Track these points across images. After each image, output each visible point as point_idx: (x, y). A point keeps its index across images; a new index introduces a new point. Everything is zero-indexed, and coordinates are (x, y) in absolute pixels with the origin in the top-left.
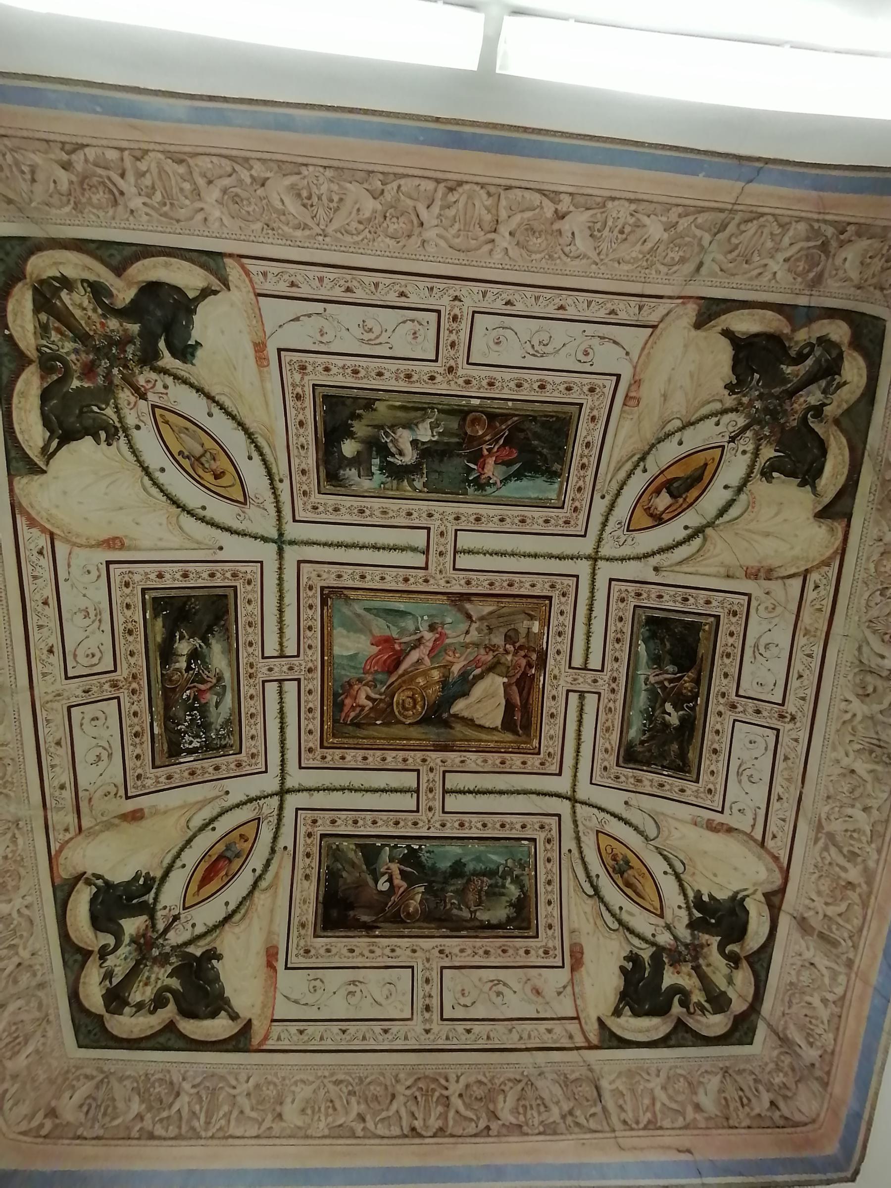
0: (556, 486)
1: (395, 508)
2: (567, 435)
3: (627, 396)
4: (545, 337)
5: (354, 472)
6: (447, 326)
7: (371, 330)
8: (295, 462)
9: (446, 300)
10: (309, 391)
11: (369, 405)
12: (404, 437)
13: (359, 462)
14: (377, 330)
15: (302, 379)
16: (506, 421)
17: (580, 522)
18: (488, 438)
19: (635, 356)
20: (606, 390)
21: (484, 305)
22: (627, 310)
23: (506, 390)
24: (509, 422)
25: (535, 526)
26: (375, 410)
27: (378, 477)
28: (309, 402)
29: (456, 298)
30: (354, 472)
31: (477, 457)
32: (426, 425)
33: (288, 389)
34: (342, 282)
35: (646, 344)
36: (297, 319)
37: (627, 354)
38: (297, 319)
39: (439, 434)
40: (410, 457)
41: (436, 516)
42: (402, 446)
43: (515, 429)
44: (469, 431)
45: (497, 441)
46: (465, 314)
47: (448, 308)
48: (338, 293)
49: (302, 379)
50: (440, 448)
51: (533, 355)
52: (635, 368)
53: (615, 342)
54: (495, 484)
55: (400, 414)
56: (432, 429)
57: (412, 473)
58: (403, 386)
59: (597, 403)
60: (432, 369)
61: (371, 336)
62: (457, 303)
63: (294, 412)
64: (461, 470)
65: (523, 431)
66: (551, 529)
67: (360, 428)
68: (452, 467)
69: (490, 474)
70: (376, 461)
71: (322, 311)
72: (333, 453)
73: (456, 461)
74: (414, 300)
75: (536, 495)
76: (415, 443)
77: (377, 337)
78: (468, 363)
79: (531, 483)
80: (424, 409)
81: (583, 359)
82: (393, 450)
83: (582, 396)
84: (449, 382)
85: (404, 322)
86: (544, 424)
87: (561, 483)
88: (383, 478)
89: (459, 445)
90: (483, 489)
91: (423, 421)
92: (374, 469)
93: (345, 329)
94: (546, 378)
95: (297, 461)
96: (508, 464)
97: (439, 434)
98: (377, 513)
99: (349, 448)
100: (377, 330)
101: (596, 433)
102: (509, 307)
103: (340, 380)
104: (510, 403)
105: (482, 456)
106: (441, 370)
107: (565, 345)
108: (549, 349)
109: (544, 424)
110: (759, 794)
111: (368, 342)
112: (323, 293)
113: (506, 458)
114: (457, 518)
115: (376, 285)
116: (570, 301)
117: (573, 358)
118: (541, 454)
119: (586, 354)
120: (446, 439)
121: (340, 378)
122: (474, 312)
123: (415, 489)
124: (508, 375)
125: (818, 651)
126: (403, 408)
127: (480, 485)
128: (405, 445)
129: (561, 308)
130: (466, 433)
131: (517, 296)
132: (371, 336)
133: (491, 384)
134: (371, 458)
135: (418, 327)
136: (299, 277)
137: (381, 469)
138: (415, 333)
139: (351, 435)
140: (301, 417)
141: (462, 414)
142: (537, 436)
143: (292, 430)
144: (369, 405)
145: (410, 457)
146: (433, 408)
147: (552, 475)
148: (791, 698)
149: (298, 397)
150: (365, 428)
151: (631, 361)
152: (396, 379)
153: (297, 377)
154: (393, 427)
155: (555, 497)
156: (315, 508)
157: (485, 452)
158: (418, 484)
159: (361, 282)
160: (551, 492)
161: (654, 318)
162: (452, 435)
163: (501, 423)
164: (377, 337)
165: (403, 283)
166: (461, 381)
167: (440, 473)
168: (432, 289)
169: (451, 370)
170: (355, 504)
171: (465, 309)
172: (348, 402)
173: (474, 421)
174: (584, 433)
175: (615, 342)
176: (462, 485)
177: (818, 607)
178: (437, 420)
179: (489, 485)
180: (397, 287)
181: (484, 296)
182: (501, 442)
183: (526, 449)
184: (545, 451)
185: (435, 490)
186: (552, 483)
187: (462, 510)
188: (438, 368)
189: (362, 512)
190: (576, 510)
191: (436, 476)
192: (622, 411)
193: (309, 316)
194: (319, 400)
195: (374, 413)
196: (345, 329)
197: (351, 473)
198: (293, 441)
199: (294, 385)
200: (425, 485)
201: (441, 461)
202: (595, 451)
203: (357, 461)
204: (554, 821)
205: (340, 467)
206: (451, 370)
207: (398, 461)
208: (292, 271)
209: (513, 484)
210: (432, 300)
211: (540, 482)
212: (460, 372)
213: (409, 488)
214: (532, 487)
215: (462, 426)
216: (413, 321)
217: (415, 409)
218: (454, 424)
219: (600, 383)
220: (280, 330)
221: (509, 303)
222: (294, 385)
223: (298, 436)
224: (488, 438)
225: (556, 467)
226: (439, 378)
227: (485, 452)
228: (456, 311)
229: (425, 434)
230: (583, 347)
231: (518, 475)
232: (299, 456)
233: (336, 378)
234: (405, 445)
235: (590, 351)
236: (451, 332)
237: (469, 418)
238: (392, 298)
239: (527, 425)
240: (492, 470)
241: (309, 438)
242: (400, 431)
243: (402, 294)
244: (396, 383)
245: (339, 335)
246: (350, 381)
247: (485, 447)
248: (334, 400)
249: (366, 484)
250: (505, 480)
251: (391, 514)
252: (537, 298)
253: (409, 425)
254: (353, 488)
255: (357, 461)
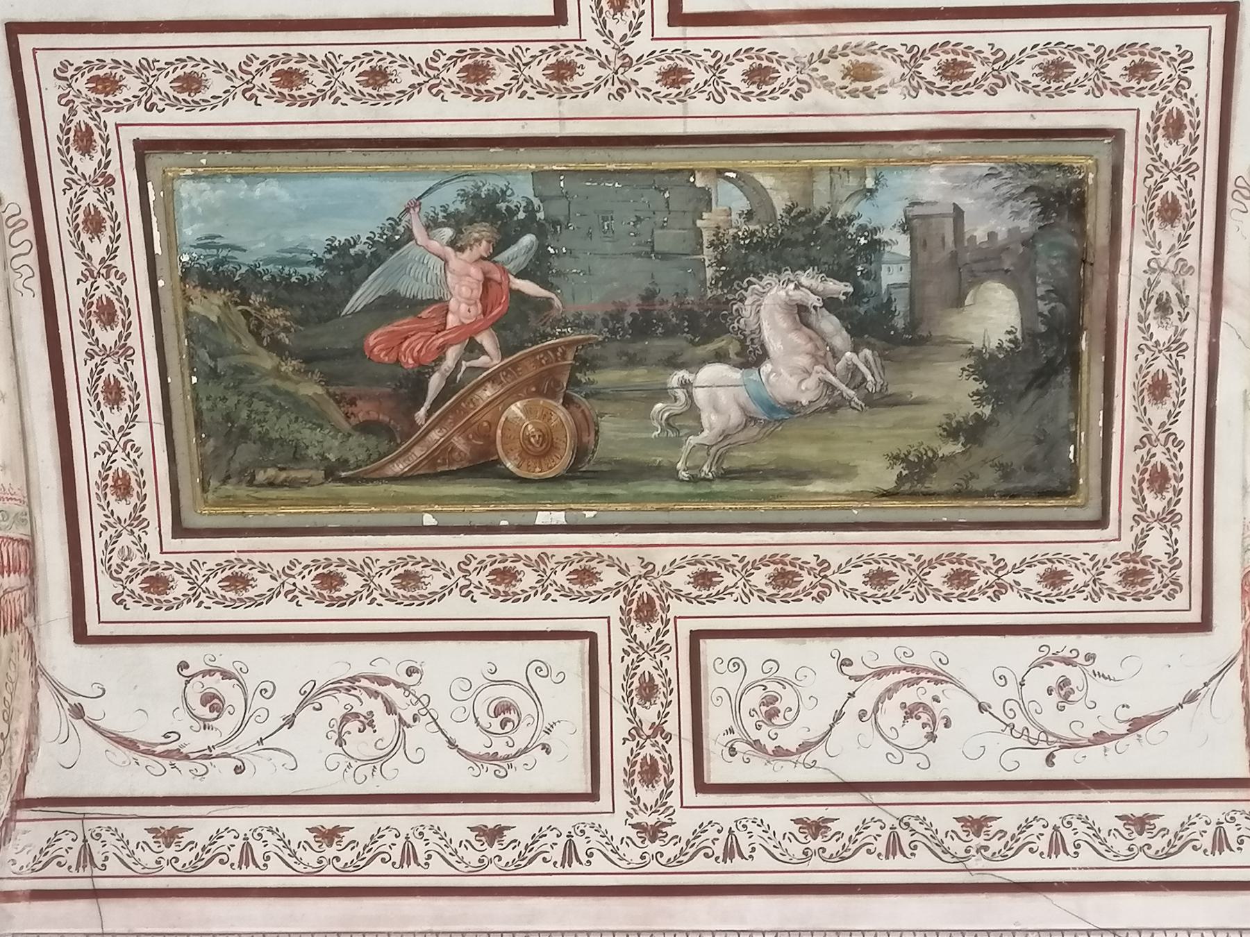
0: (190, 233)
1: (818, 97)
2: (199, 423)
3: (32, 572)
4: (360, 743)
5: (978, 230)
6: (672, 748)
7: (910, 712)
8: (1198, 251)
9: (685, 823)
10: (1123, 505)
11: (916, 476)
12: (789, 373)
13: (958, 267)
14: (891, 714)
15: (1140, 542)
16: (431, 459)
17: (52, 90)
18: (488, 393)
19: (52, 715)
20: (108, 587)
21: (564, 820)
22: (127, 844)
23: (452, 560)
24: (418, 452)
25: (233, 58)
26: (895, 458)
27: (884, 215)
28: (1126, 465)
29: (653, 833)
30: (978, 230)
31: (516, 321)
32: (712, 422)
33: (1189, 505)
34: (996, 845)
35: (29, 747)
36: (1137, 725)
37: (78, 712)
38: (1137, 725)
39: (662, 393)
40: (768, 304)
41: (648, 76)
42: (798, 339)
43: (390, 432)
44: (561, 413)
45: (451, 385)
46: (620, 788)
47: (674, 800)
48: (1008, 813)
49: (1140, 542)
50: (658, 346)
51: (385, 681)
52: (38, 671)
53: (131, 744)
54: (432, 225)
55: (807, 452)
56: (692, 410)
57: (758, 245)
58: (804, 547)
59: (126, 540)
60: (709, 609)
61: (908, 695)
62: (651, 820)
63: (1181, 429)
64: (567, 265)
65: (366, 428)
66: (164, 50)
67: (949, 389)
68: (599, 281)
69: (457, 261)
70: (893, 275)
71: (1062, 756)
72: (1057, 293)
73: (591, 302)
74: (781, 817)
75: (260, 190)
76: (752, 355)
77: (889, 692)
78: (592, 637)
79: (292, 237)
80: (727, 475)
81: (215, 683)
82: (829, 323)
83: (185, 560)
84: (648, 570)
85: (805, 747)
86: (297, 456)
87: (172, 244)
88: (867, 213)
89: (584, 363)
90: (471, 198)
91: (725, 435)
92: (901, 245)
93: (986, 711)
94: (321, 611)
95: (1190, 253)
96: (391, 305)
97: (662, 393)
98: (892, 69)
99: (994, 316)
100: (891, 714)
101: (96, 438)
102: (491, 822)
103: (1012, 547)
104: (429, 520)
105: (499, 326)
106: (678, 607)
107: (288, 719)
108: (335, 706)
109: (297, 456)
110: (311, 760)
111: (917, 675)
112: (1051, 810)
113: (403, 324)
114: (563, 71)
115: (894, 847)
116: (310, 857)
117: (251, 683)
118: (276, 347)
119: (212, 701)
120: (639, 376)
121: (1012, 555)
122: (593, 796)
123: (743, 181)
124: (453, 610)
125: (921, 864)
126: (800, 474)
127: (489, 216)
128: (788, 341)
129: (329, 836)
130: (568, 402)
131: (472, 857)
132: (908, 695)
133: (506, 576)
134: (913, 287)
135: (762, 736)
136: (1120, 845)
137: (875, 246)
138: (771, 715)
139: (986, 366)
140: (1158, 414)
141: (586, 470)
142: (302, 409)
143: (1194, 366)
144: (916, 476)
145: (768, 304)
146: (694, 480)
147: (212, 274)
148: (727, 813)
149: (1159, 479)
150: (936, 395)
151: (59, 691)
152: (824, 564)
153: (1156, 546)
154: (835, 405)
155: (185, 189)
156: (1141, 70)
157: (486, 340)
158: (730, 200)
159: (938, 847)
160: (202, 204)
161: (32, 833)
162: (616, 395)
163: (445, 449)
164: (889, 692)
165: (816, 863)
166: (610, 577)
167: (650, 251)
168: (729, 854)
169: (647, 611)
170: (978, 100)
171: (623, 803)
172: (988, 478)
173: (547, 446)
174: (139, 434)
175: (131, 744)
176: (558, 209)
177: (258, 850)
178: (678, 443)
179: (456, 221)
180: (833, 847)
181: (570, 845)
182: (435, 383)
183: (337, 365)
184: (267, 361)
185: (657, 169)
186: (208, 243)
187: (544, 106)
188: (687, 614)
189: (953, 71)
190: (85, 141)
191: (666, 240)
192: (28, 518)
193: (1100, 738)
194: (1089, 478)
195: (899, 446)
196: (986, 711)
197: (992, 221)
198: (1196, 333)
199: (1169, 517)
200: (705, 199)
201: (649, 297)
202: (78, 373)
203: (966, 269)
204: (104, 613)
205: (1029, 242)
206: (647, 611)
207: (812, 285)
208: (1141, 860)
209: (360, 228)
210: (726, 818)
211: (257, 247)
212: (612, 607)
213: (767, 181)
214: (284, 220)
215: (587, 426)
216: (780, 753)
217: (754, 478)
218: (616, 434)
219: (138, 611)
220: (1196, 685)
221: (493, 835)
222: (1169, 517)
223: (1177, 345)
224: (488, 393)
225: (210, 306)
226: (680, 580)
227: (486, 340)
228: (648, 795)
229: (716, 389)
230: (227, 724)
231: (348, 265)
232: (1183, 268)
233: (1027, 552)
234: (788, 341)
235: (204, 712)
236: (658, 729)
237: (562, 462)
238: (847, 816)
239: (357, 448)
240: (454, 277)
241: (1135, 338)
242: (806, 392)
243: (816, 828)
244: (824, 553)
245: (1011, 690)
246: (980, 547)
247: (491, 359)
248: (1037, 481)
249: (931, 186)
250: (393, 241)
251: (833, 71)
252: (409, 855)
253: (777, 415)
254: (983, 168)
255: (966, 269)
